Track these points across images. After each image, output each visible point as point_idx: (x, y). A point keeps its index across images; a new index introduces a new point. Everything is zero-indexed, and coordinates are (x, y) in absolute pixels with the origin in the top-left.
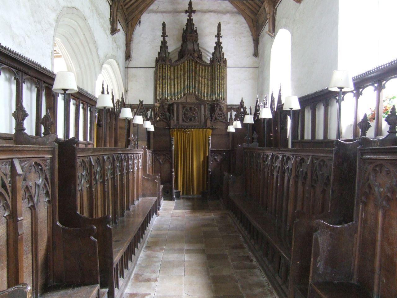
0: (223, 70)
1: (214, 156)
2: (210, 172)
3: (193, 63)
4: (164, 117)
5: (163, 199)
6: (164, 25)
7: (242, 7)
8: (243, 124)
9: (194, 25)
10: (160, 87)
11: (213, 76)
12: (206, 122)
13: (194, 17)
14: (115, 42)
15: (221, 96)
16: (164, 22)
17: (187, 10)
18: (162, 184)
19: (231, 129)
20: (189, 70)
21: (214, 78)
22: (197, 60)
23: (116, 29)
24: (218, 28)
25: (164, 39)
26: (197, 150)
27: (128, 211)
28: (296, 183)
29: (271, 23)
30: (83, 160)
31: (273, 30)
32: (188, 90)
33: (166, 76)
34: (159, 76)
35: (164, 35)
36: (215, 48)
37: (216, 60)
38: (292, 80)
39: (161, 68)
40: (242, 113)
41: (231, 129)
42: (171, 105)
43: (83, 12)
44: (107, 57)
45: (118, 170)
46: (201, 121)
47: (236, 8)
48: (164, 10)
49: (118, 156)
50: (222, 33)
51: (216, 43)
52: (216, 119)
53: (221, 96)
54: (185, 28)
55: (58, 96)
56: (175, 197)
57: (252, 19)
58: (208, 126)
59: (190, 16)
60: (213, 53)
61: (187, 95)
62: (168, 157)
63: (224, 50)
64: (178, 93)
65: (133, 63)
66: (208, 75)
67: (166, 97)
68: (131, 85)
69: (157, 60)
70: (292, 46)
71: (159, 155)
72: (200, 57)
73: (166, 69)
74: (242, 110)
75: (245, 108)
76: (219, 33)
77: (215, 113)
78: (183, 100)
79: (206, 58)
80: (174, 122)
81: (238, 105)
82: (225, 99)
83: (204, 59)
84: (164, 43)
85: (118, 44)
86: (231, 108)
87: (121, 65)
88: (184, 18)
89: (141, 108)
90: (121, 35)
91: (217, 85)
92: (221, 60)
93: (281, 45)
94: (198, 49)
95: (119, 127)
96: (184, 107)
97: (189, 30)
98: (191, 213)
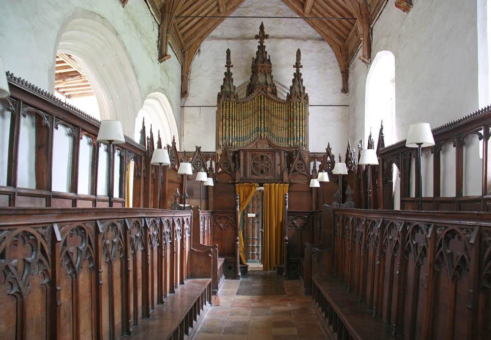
0: (304, 109)
1: (292, 220)
2: (287, 241)
3: (266, 100)
4: (228, 168)
5: (223, 277)
6: (228, 52)
7: (327, 32)
8: (331, 175)
9: (266, 53)
10: (223, 129)
11: (290, 116)
12: (282, 173)
13: (266, 43)
14: (166, 71)
15: (301, 140)
16: (228, 49)
17: (258, 34)
18: (221, 256)
19: (315, 183)
20: (260, 108)
21: (292, 118)
22: (270, 96)
23: (166, 55)
24: (297, 56)
25: (228, 70)
26: (262, 211)
27: (160, 306)
28: (435, 276)
29: (366, 49)
30: (168, 220)
31: (369, 56)
32: (259, 133)
33: (231, 115)
34: (221, 116)
35: (229, 65)
36: (294, 81)
37: (295, 95)
38: (398, 116)
39: (224, 105)
40: (329, 163)
41: (315, 183)
42: (238, 152)
43: (113, 22)
44: (151, 89)
45: (167, 237)
46: (275, 174)
47: (319, 33)
48: (230, 36)
49: (154, 220)
50: (302, 62)
51: (295, 75)
52: (295, 171)
53: (301, 140)
54: (255, 56)
55: (82, 138)
56: (240, 274)
57: (340, 46)
58: (285, 181)
59: (261, 42)
60: (291, 87)
61: (257, 140)
62: (231, 220)
63: (304, 84)
64: (247, 138)
65: (190, 101)
66: (284, 114)
67: (231, 142)
68: (187, 128)
69: (219, 96)
70: (396, 71)
71: (220, 218)
72: (274, 92)
73: (231, 107)
74: (329, 159)
75: (333, 156)
76: (298, 62)
77: (293, 163)
78: (251, 147)
79: (282, 94)
80: (239, 175)
81: (323, 153)
82: (306, 146)
83: (279, 95)
84: (228, 75)
85: (170, 75)
86: (314, 157)
87: (174, 102)
88: (256, 43)
89: (197, 157)
90: (173, 63)
91: (296, 127)
92: (300, 95)
93: (381, 76)
94: (271, 83)
95: (169, 181)
96: (253, 156)
97: (260, 59)
98: (259, 301)
